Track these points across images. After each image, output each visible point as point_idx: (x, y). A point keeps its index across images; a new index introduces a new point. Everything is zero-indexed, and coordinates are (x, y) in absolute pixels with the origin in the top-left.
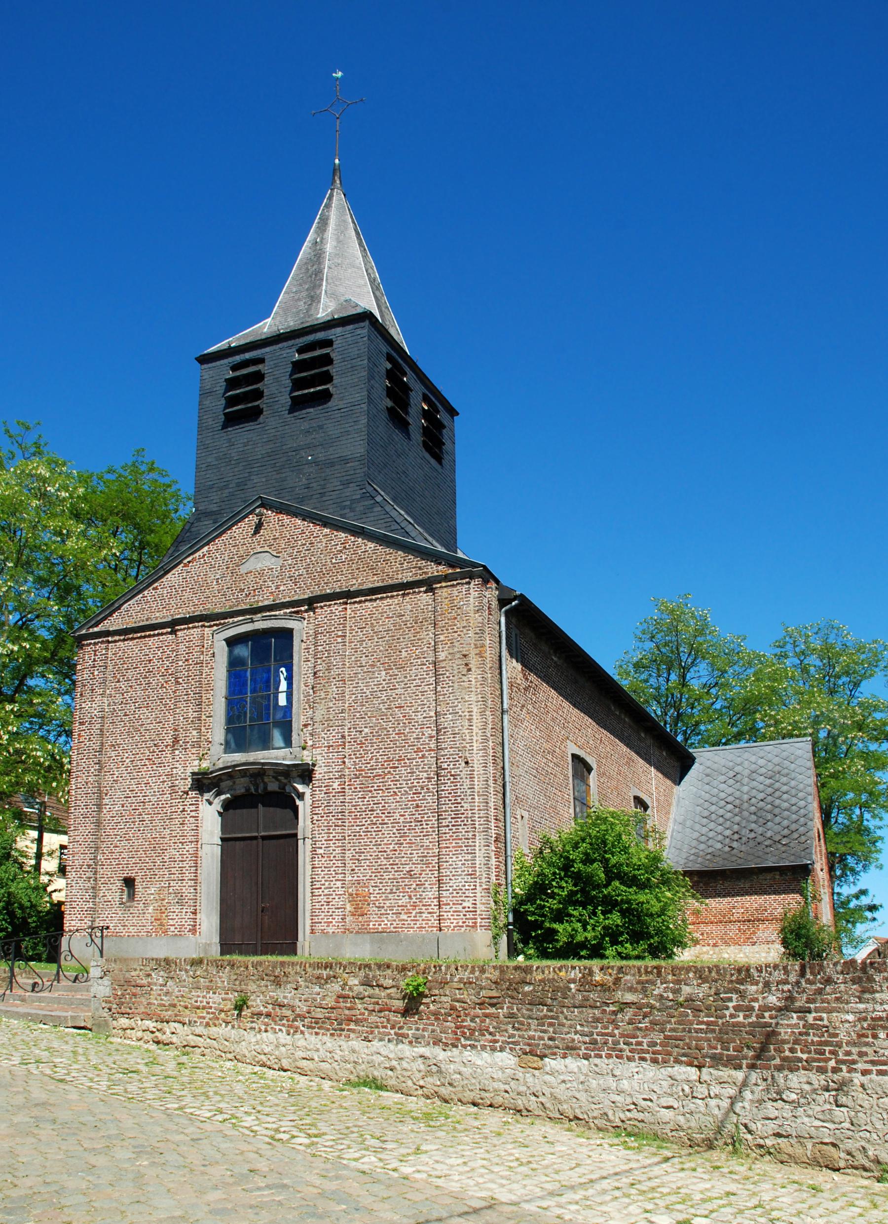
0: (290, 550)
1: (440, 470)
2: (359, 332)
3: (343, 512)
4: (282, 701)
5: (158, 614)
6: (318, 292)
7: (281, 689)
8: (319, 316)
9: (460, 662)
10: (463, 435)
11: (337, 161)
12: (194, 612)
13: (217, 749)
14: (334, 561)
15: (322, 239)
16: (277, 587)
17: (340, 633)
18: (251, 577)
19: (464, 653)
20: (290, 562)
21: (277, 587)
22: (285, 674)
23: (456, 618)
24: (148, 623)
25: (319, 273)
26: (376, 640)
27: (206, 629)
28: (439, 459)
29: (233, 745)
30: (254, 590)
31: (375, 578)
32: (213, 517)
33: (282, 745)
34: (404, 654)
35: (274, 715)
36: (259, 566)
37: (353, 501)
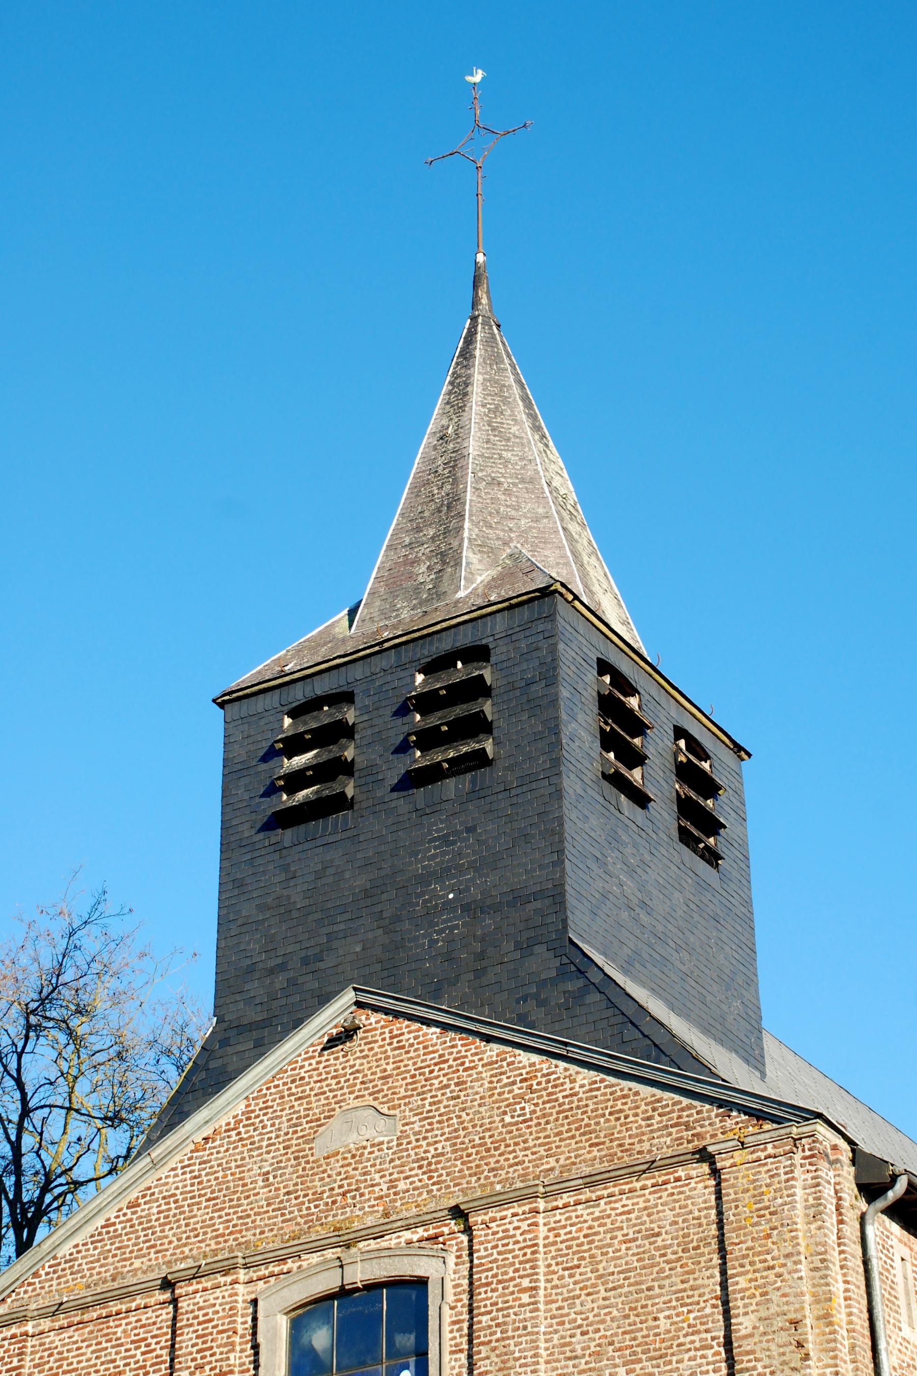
0: (416, 1101)
1: (716, 884)
2: (541, 627)
3: (522, 1008)
5: (137, 1263)
6: (455, 544)
8: (461, 594)
9: (783, 1337)
10: (760, 804)
11: (480, 258)
12: (215, 1252)
14: (508, 1119)
15: (459, 427)
16: (392, 1184)
17: (526, 1283)
18: (336, 1165)
19: (792, 1316)
21: (392, 1184)
23: (769, 1236)
24: (116, 1285)
25: (452, 506)
26: (603, 1294)
28: (712, 857)
30: (344, 1194)
31: (595, 1153)
32: (255, 1034)
34: (663, 1324)
36: (352, 1140)
37: (542, 984)
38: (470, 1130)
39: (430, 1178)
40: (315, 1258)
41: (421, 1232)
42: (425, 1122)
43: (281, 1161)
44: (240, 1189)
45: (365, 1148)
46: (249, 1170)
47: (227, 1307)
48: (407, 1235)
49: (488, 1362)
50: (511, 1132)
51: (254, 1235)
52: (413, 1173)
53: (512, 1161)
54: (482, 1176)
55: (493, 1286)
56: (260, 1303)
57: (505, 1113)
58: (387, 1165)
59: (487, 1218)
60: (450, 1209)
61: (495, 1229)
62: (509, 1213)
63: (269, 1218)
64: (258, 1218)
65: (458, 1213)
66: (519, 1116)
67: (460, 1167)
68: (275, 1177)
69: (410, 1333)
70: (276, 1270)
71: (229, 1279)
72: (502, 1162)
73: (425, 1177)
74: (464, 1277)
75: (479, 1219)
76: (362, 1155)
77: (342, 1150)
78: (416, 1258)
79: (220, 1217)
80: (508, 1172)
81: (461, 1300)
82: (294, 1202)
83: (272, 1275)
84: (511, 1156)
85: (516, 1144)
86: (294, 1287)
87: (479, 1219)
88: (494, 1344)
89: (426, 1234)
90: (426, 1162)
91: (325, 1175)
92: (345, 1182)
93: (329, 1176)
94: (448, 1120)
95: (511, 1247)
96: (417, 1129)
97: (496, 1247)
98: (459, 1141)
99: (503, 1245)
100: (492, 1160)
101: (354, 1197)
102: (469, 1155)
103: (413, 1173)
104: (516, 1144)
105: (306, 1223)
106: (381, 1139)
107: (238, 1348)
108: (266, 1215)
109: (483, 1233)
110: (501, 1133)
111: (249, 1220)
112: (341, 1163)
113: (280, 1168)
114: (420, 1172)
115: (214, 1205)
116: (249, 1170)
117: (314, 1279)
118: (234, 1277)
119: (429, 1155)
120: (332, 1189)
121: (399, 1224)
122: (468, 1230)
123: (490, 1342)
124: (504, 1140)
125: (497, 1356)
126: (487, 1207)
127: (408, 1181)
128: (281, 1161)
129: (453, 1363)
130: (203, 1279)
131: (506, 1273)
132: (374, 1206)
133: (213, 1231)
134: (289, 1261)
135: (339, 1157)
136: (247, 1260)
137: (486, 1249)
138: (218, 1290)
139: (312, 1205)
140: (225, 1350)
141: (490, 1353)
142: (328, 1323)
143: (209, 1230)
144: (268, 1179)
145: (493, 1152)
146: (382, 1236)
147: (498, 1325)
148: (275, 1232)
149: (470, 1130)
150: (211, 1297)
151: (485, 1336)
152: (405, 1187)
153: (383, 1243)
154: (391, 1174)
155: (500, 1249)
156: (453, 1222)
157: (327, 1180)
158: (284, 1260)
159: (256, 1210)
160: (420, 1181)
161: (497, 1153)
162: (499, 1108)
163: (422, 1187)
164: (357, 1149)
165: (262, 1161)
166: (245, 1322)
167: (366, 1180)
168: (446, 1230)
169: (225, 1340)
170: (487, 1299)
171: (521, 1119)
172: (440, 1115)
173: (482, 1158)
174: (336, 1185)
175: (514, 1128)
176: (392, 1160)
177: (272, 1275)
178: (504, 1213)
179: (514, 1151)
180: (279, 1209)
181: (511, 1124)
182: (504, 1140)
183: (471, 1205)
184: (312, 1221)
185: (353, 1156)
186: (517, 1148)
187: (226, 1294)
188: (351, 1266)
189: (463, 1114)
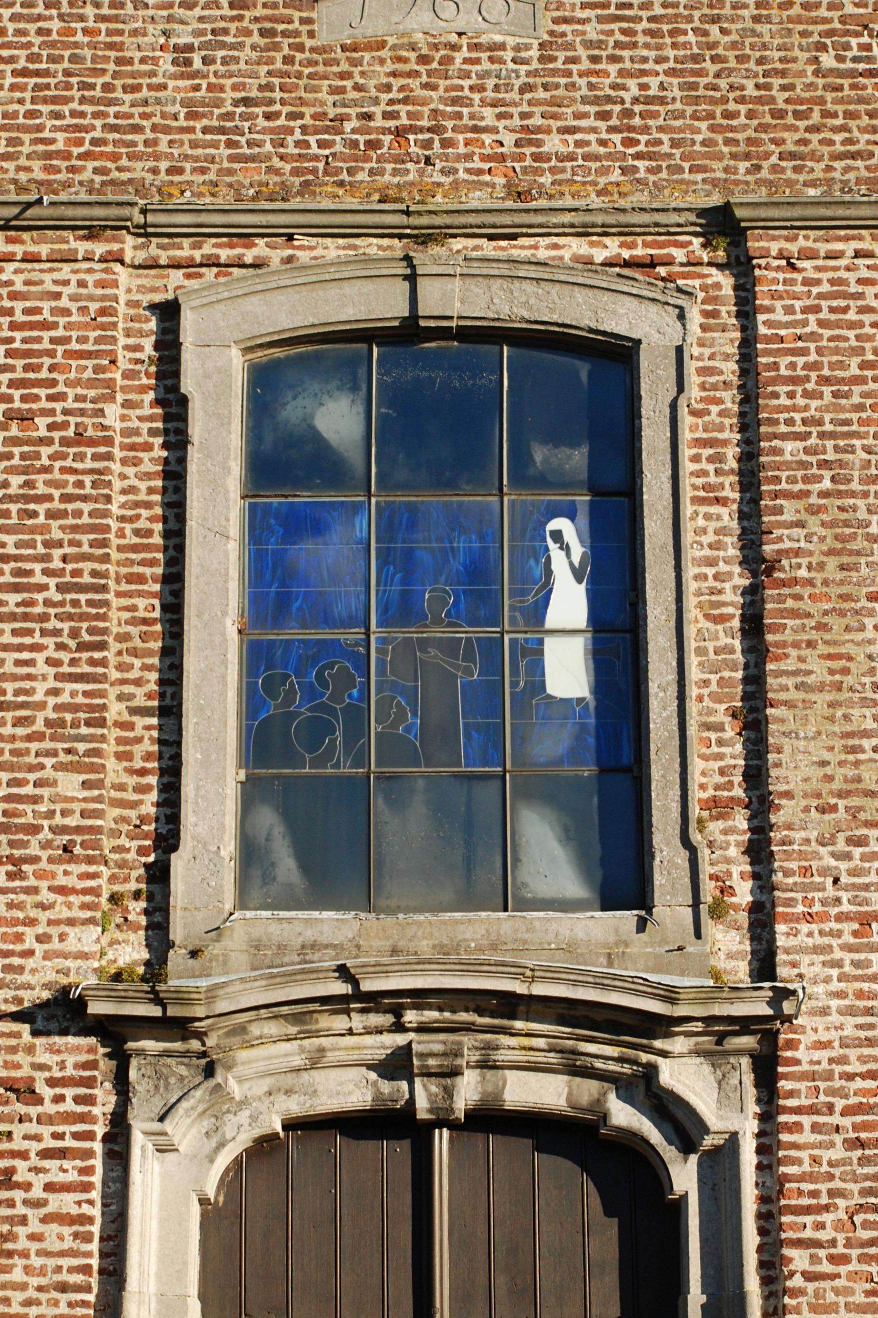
4: (567, 671)
7: (554, 618)
13: (72, 935)
14: (828, 60)
16: (528, 136)
18: (376, 71)
20: (592, 31)
22: (578, 551)
27: (122, 273)
29: (287, 866)
33: (572, 886)
35: (520, 740)
38: (732, 63)
39: (629, 142)
40: (332, 249)
41: (612, 247)
42: (615, 26)
43: (226, 32)
44: (112, 67)
45: (455, 47)
46: (134, 33)
47: (94, 306)
48: (577, 246)
49: (797, 532)
50: (840, 88)
51: (155, 171)
52: (583, 123)
53: (839, 148)
54: (765, 164)
55: (810, 386)
56: (188, 320)
57: (823, 48)
58: (515, 96)
59: (793, 248)
60: (702, 213)
61: (813, 275)
62: (849, 248)
63: (194, 144)
64: (164, 138)
65: (723, 226)
66: (855, 60)
67: (705, 134)
68: (206, 61)
69: (574, 445)
70: (225, 254)
71: (99, 248)
72: (814, 145)
73: (617, 138)
74: (727, 357)
75: (774, 247)
76: (447, 61)
77: (391, 41)
78: (606, 297)
79: (57, 116)
80: (829, 169)
81: (720, 401)
82: (261, 122)
83: (211, 262)
84: (838, 138)
85: (850, 115)
86: (278, 297)
87: (774, 247)
88: (813, 500)
89: (626, 254)
90: (617, 108)
91: (348, 84)
92: (403, 109)
93: (357, 88)
94: (673, 33)
95: (852, 316)
96: (593, 36)
97: (817, 309)
98: (703, 81)
99: (832, 310)
100: (790, 137)
101: (427, 145)
102: (728, 115)
103: (583, 123)
104: (849, 115)
105: (295, 172)
106: (498, 38)
107: (120, 397)
108: (186, 137)
109: (781, 276)
110: (811, 86)
111: (139, 138)
112: (389, 67)
113: (223, 45)
114: (602, 125)
115: (37, 87)
116: (134, 33)
117: (333, 291)
118: (116, 247)
119: (627, 97)
120: (369, 117)
121: (567, 218)
122: (742, 266)
123: (808, 494)
124: (822, 101)
125: (823, 524)
126: (794, 227)
127: (571, 139)
128: (226, 32)
129: (701, 522)
130: (26, 236)
131: (841, 366)
132: (480, 172)
133: (36, 141)
134: (198, 260)
135: (385, 53)
136: (151, 218)
137: (789, 310)
138: (67, 267)
139: (312, 140)
140: (92, 393)
141: (804, 516)
142: (355, 388)
143: (26, 137)
144: (188, 62)
145: (790, 120)
146: (514, 237)
147: (824, 464)
148: (212, 176)
149: (732, 63)
150: (47, 278)
151: (792, 480)
152: (563, 149)
153: (520, 249)
154: (524, 116)
155: (824, 315)
156: (697, 242)
157: (353, 95)
158: (246, 238)
159: (157, 120)
160: (603, 143)
161: (802, 124)
162: (804, 34)
163: (609, 156)
164: (436, 47)
165: (170, 19)
166: (138, 348)
167: (459, 116)
168: (679, 255)
169: (89, 374)
170: (794, 408)
171: (861, 66)
172: (650, 19)
173: (763, 128)
174: (377, 111)
175: (846, 82)
176: (526, 88)
177: (211, 262)
178: (838, 246)
179: (844, 128)
180: (222, 131)
181: (832, 72)
182: (822, 101)
183: (763, 213)
184: (314, 171)
185: (424, 60)
186: (852, 124)
187: (90, 279)
188: (438, 282)
189: (714, 30)
